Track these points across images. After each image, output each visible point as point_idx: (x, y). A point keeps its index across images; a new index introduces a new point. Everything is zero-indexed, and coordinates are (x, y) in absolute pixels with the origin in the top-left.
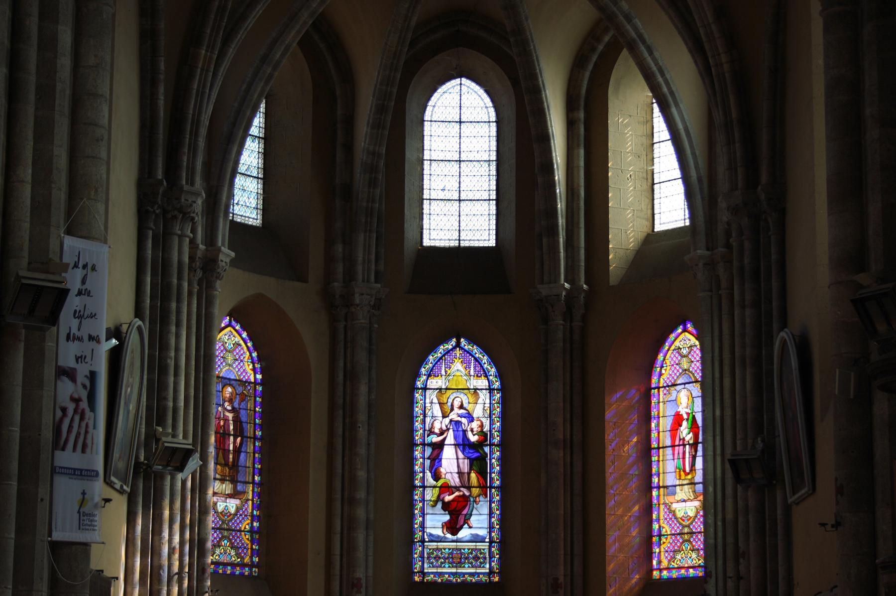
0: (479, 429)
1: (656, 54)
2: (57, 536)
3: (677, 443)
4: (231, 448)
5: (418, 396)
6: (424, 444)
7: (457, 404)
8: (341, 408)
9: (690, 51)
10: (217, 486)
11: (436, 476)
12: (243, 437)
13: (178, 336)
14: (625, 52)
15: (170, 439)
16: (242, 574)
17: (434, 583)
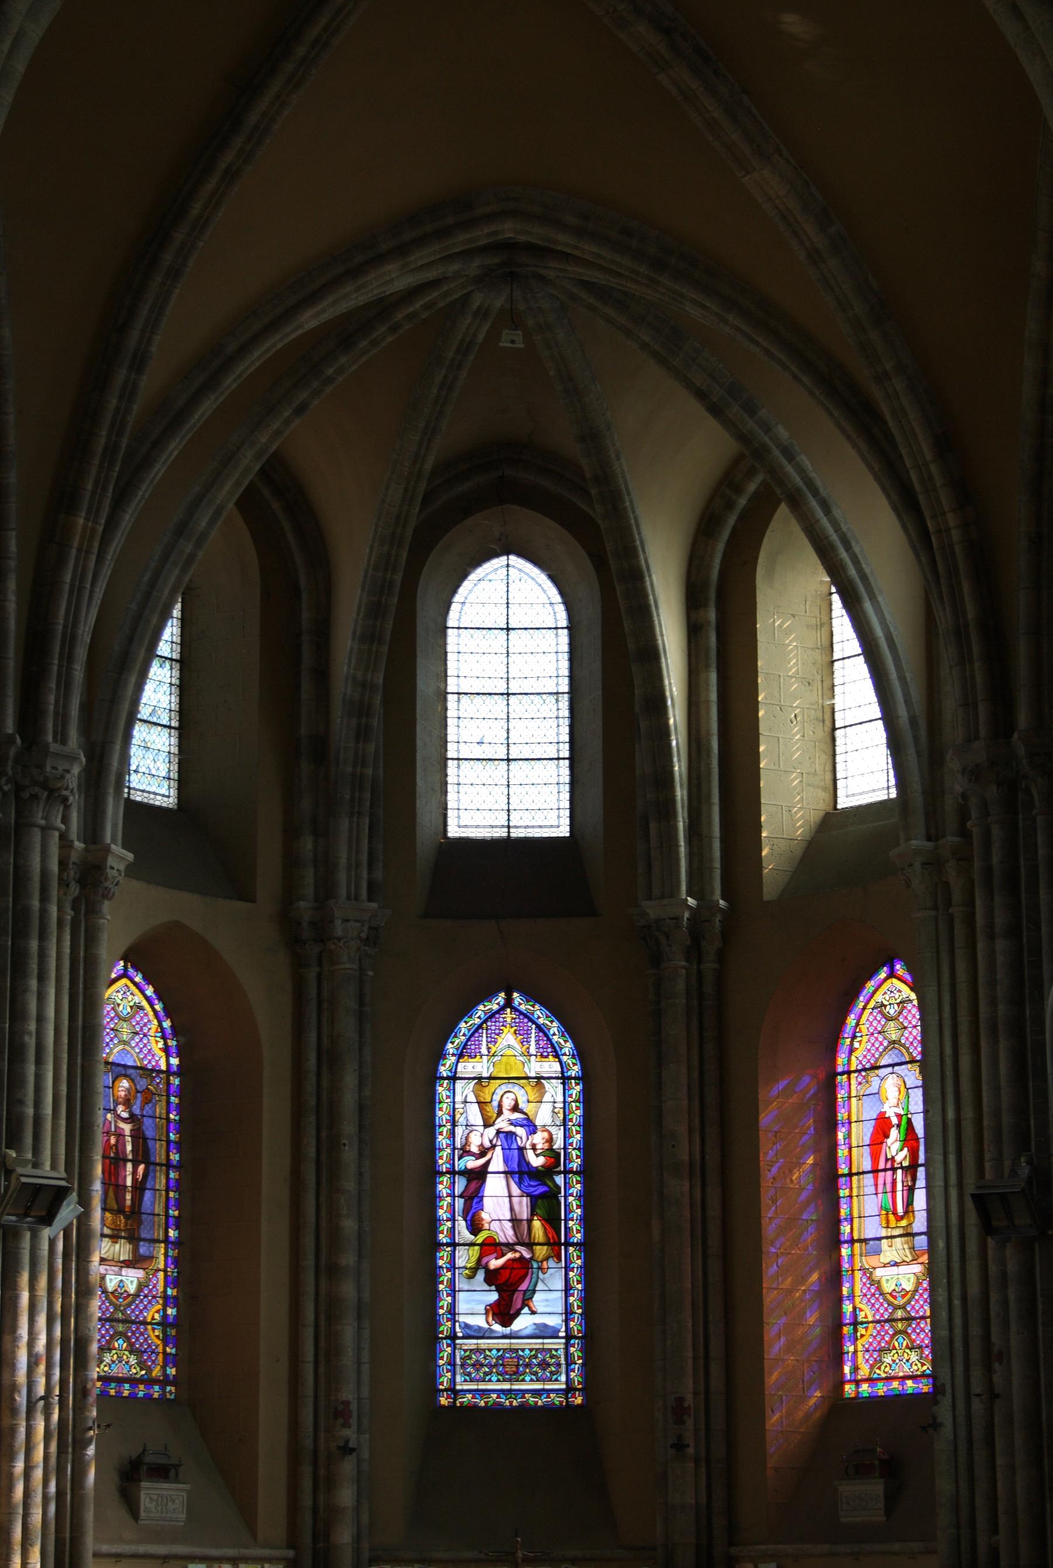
0: (546, 1146)
1: (837, 513)
3: (881, 1166)
5: (442, 1091)
6: (452, 1172)
7: (508, 1103)
8: (314, 1114)
9: (895, 508)
10: (105, 1248)
11: (475, 1227)
13: (41, 997)
14: (783, 509)
16: (148, 1397)
17: (474, 1407)
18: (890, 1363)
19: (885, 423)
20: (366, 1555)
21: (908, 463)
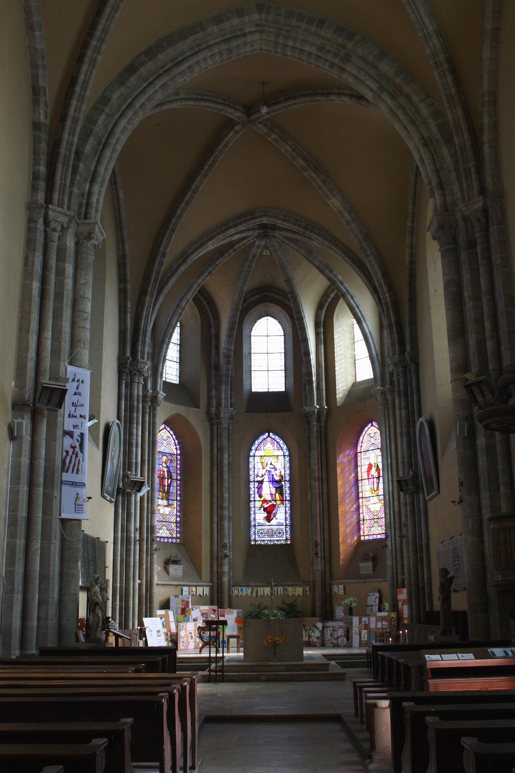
1: (355, 299)
2: (64, 516)
3: (370, 477)
4: (166, 484)
5: (251, 459)
6: (254, 481)
7: (269, 463)
8: (216, 466)
9: (371, 293)
10: (160, 502)
11: (260, 496)
12: (172, 479)
13: (137, 429)
14: (342, 300)
15: (134, 477)
16: (172, 542)
18: (374, 529)
19: (368, 270)
20: (232, 584)
21: (375, 280)
